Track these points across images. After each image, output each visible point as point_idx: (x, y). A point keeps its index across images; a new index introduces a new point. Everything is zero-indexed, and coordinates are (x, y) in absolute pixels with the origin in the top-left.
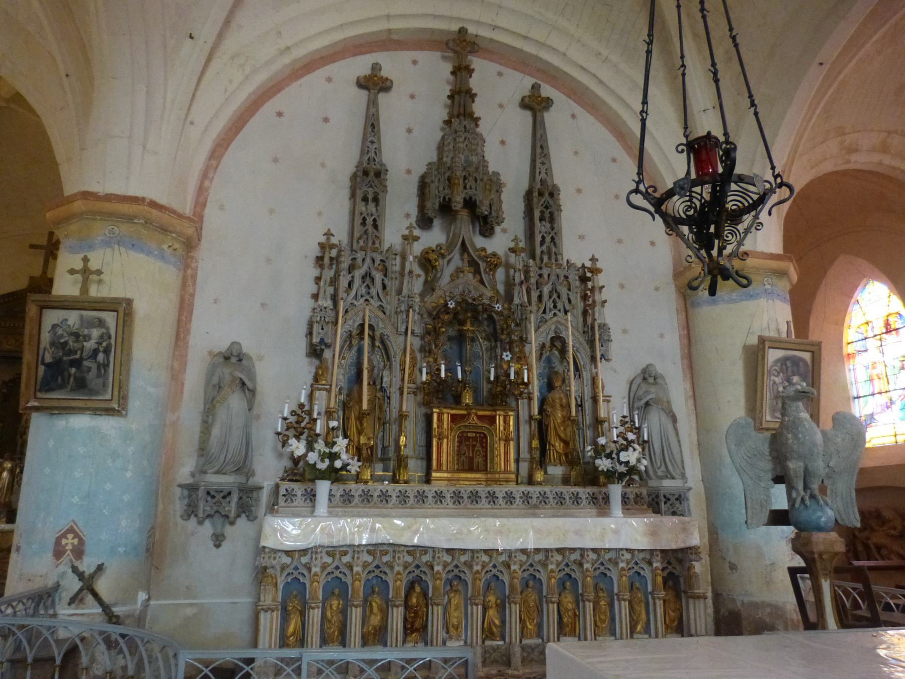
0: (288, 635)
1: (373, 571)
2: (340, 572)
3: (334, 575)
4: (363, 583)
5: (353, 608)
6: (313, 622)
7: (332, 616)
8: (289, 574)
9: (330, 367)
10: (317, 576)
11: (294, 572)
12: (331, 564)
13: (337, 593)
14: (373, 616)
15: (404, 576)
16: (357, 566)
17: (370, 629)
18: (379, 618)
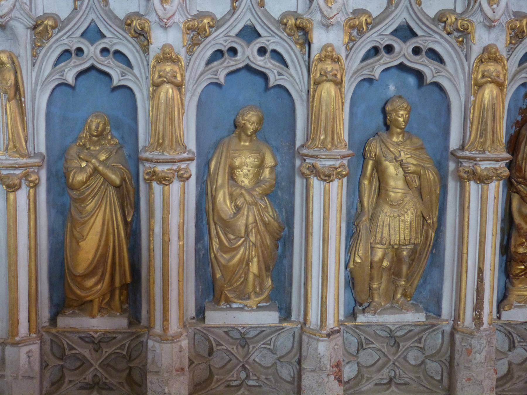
0: (81, 268)
1: (389, 49)
2: (262, 51)
3: (240, 61)
4: (349, 89)
5: (315, 182)
6: (165, 232)
7: (238, 209)
8: (66, 54)
9: (339, 132)
10: (175, 61)
11: (397, 45)
12: (224, 20)
13: (251, 128)
14: (387, 209)
15: (512, 65)
16: (327, 26)
17: (379, 253)
18: (409, 216)
